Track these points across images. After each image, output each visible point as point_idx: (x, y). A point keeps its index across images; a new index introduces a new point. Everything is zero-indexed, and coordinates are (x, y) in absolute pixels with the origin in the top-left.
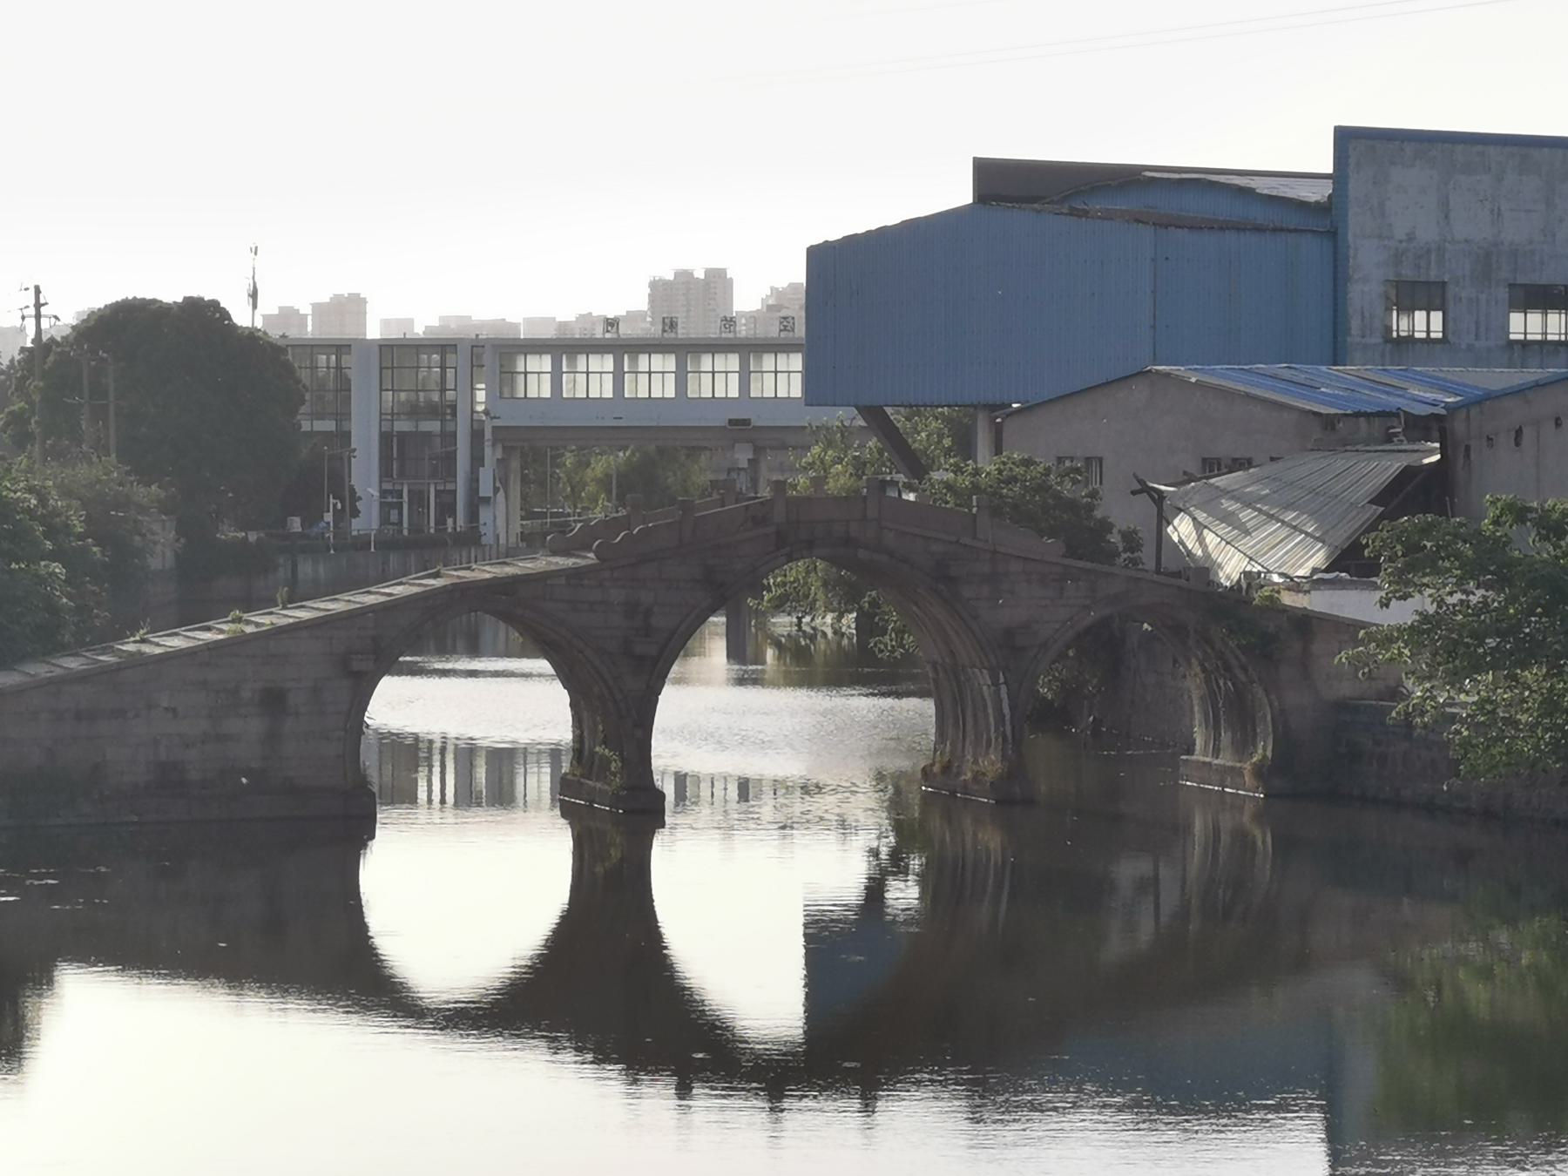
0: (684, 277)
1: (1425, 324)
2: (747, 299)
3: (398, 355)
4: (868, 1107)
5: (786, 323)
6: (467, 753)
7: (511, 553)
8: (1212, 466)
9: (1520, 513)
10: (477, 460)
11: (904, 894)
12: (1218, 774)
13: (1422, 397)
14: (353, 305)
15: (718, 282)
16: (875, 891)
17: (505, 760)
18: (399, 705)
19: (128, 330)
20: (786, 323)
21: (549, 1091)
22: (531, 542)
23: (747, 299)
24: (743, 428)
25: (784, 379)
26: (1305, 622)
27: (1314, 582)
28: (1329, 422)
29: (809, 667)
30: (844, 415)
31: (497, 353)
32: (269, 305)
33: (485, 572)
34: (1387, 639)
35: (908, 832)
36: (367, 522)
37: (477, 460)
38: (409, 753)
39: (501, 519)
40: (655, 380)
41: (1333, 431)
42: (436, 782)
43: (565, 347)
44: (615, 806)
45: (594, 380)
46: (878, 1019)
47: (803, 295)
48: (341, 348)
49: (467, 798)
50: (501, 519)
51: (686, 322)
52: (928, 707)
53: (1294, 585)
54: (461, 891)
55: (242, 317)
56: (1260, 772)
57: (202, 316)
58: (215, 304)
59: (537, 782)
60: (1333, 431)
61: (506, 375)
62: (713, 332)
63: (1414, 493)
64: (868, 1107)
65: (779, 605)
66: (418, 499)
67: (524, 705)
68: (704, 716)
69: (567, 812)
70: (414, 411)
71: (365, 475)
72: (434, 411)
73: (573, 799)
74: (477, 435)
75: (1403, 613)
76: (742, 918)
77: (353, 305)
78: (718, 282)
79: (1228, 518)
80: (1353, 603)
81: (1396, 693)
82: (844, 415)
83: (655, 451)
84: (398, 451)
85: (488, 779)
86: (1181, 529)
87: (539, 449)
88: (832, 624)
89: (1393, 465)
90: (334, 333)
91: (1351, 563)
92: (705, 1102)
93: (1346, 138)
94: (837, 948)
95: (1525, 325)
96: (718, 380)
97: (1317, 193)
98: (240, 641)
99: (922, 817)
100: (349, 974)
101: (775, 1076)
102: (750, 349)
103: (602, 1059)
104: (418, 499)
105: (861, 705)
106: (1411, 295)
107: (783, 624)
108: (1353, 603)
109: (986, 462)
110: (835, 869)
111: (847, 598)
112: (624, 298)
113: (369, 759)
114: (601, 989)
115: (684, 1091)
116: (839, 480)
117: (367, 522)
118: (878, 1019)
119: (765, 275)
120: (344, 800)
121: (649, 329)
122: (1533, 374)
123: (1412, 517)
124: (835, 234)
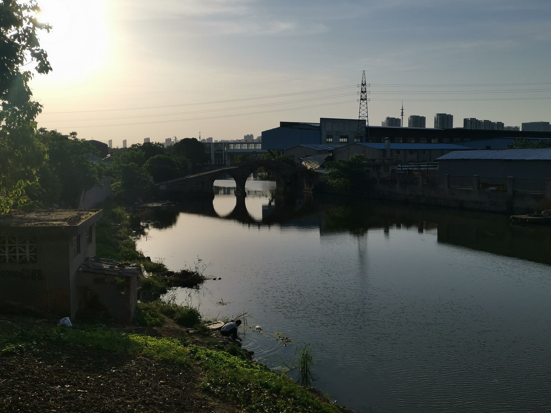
0: (248, 135)
1: (330, 140)
2: (255, 138)
3: (216, 144)
4: (269, 227)
5: (259, 141)
6: (224, 188)
7: (229, 166)
8: (307, 156)
9: (341, 161)
10: (225, 156)
11: (273, 204)
12: (307, 190)
13: (330, 148)
14: (211, 139)
15: (252, 136)
16: (270, 203)
17: (229, 189)
18: (218, 183)
19: (186, 141)
20: (259, 141)
21: (235, 227)
22: (231, 165)
23: (255, 138)
24: (255, 152)
25: (259, 147)
26: (317, 173)
27: (318, 169)
28: (320, 151)
29: (262, 178)
30: (266, 151)
31: (227, 144)
32: (202, 139)
33: (227, 168)
34: (326, 175)
35: (273, 197)
36: (213, 163)
37: (225, 156)
38: (218, 189)
39: (228, 163)
40: (245, 147)
41: (320, 152)
42: (222, 192)
43: (235, 143)
44: (241, 194)
45: (238, 147)
46: (271, 217)
47: (261, 139)
48: (210, 144)
49: (225, 193)
50: (228, 163)
51: (248, 139)
52: (275, 182)
53: (316, 169)
54: (224, 204)
55: (199, 140)
56: (312, 190)
57: (194, 140)
58: (286, 127)
59: (233, 192)
60: (320, 152)
61: (228, 146)
62: (251, 141)
63: (329, 159)
64: (269, 227)
65: (259, 172)
66: (219, 160)
67: (231, 183)
68: (251, 184)
69: (236, 195)
70: (218, 150)
71: (213, 158)
72: (220, 151)
73: (236, 194)
74: (225, 153)
75: (328, 172)
76: (255, 206)
77: (211, 139)
78: (252, 136)
79: (309, 162)
80: (323, 171)
81: (327, 181)
82: (266, 151)
83: (245, 155)
84: (216, 155)
85: (227, 191)
86: (303, 163)
87: (232, 155)
88: (265, 174)
89: (327, 156)
90: (209, 142)
91: (322, 167)
92: (251, 227)
93: (322, 119)
94: (266, 210)
95: (341, 140)
96: (252, 147)
97: (318, 125)
98: (198, 176)
99: (275, 195)
100: (212, 214)
101: (258, 224)
102: (255, 143)
103: (240, 222)
104: (219, 160)
105: (268, 182)
106: (329, 137)
107: (259, 174)
108: (323, 171)
109: (282, 156)
110: (266, 201)
111: (266, 171)
112: (241, 138)
113: (214, 189)
114: (240, 215)
115: (249, 226)
116: (265, 158)
117: (213, 163)
118: (271, 217)
119: (257, 135)
120: (212, 193)
121: (244, 141)
122: (342, 145)
123: (329, 162)
124: (481, 118)
